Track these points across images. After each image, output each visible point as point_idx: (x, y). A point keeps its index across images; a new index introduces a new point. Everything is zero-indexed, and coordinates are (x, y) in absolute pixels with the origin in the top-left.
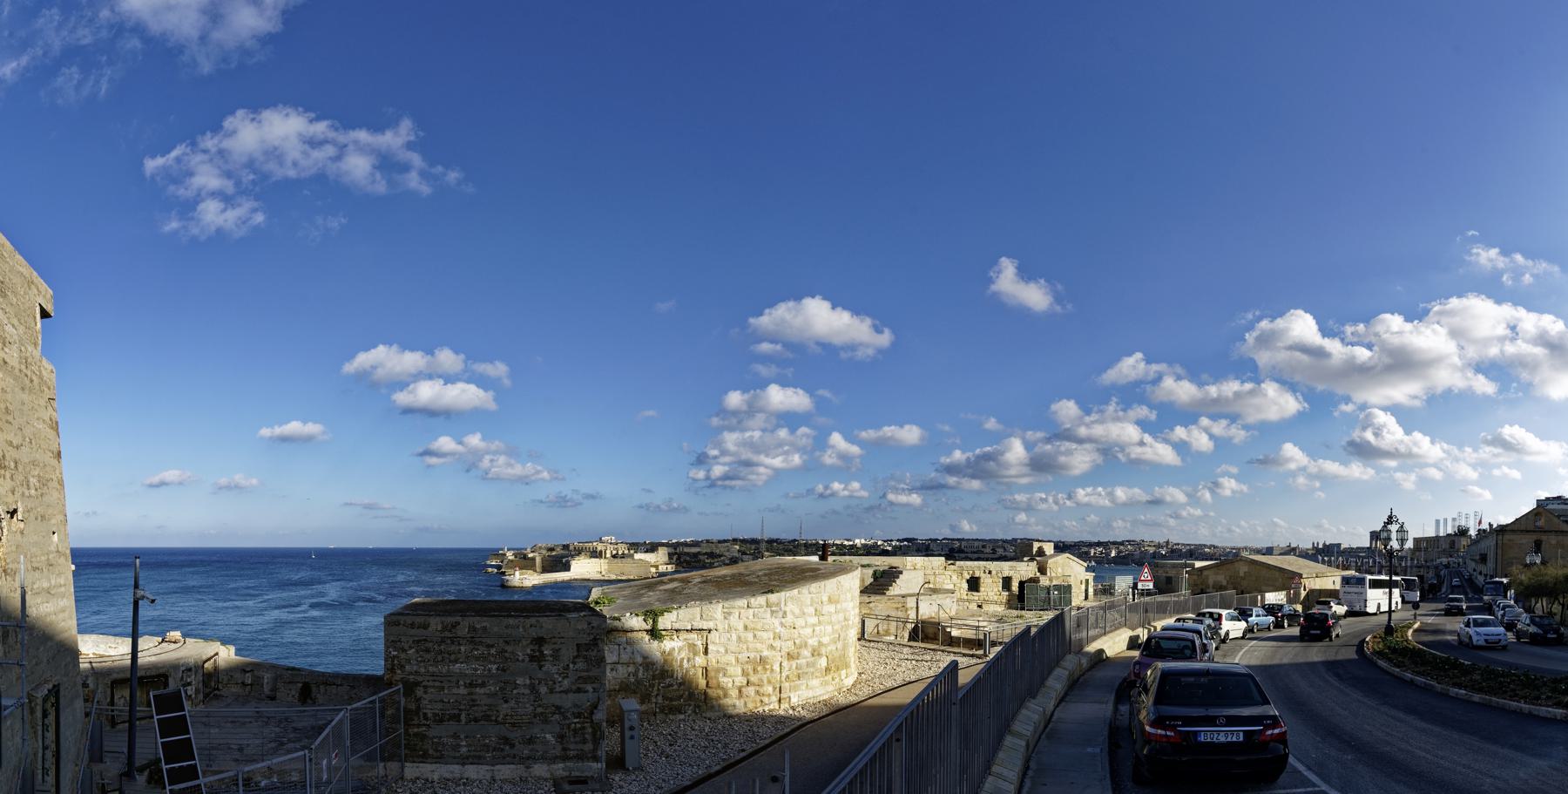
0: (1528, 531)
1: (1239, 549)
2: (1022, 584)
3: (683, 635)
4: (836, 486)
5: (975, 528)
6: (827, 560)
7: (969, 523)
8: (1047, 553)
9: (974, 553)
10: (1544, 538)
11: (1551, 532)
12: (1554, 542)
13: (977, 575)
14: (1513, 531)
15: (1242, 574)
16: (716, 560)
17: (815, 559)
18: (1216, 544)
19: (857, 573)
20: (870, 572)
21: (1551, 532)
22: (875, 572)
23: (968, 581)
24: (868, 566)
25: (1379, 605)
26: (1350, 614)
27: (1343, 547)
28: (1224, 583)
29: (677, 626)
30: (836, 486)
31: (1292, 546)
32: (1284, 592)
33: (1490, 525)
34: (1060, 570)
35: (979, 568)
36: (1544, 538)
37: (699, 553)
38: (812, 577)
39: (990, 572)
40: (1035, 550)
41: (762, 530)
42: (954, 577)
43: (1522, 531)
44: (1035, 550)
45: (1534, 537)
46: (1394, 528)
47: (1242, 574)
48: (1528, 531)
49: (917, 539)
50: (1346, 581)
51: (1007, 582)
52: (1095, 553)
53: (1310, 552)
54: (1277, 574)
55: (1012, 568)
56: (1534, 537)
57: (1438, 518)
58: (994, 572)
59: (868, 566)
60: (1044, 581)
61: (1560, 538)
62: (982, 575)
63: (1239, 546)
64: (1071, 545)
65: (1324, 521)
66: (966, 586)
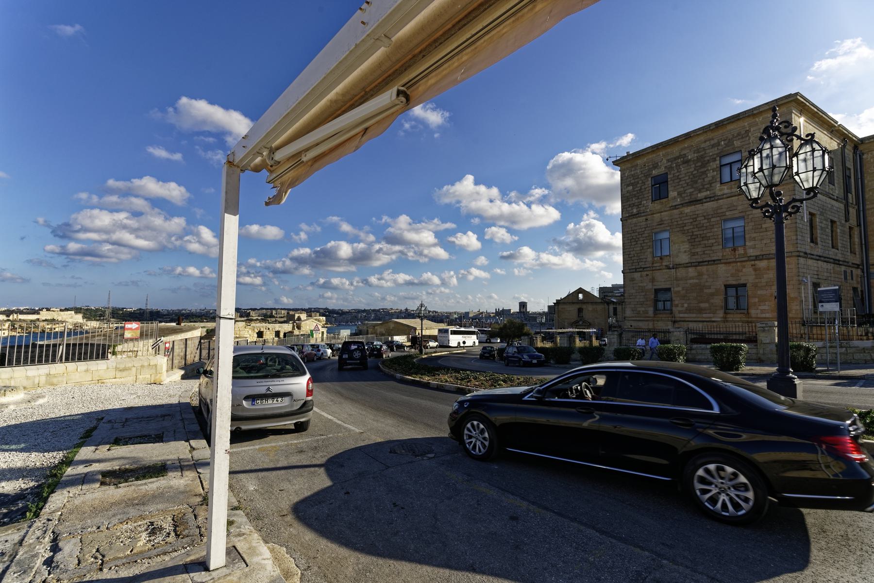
0: (573, 303)
1: (451, 313)
2: (285, 334)
3: (126, 354)
4: (192, 270)
5: (291, 301)
6: (180, 325)
7: (287, 298)
8: (302, 319)
9: (282, 317)
10: (584, 307)
11: (588, 303)
12: (590, 309)
13: (262, 330)
14: (564, 303)
15: (391, 328)
16: (57, 325)
17: (174, 324)
18: (437, 310)
19: (200, 329)
20: (205, 330)
21: (588, 303)
22: (207, 330)
23: (257, 333)
24: (204, 327)
25: (474, 342)
26: (441, 346)
27: (512, 311)
28: (384, 332)
29: (124, 350)
30: (192, 270)
31: (481, 311)
32: (406, 336)
33: (523, 305)
34: (308, 327)
35: (263, 327)
36: (584, 307)
37: (38, 320)
38: (870, 139)
39: (269, 329)
40: (296, 318)
41: (109, 298)
42: (250, 332)
43: (570, 303)
44: (296, 318)
45: (578, 306)
46: (423, 309)
47: (391, 328)
48: (573, 303)
49: (241, 309)
50: (440, 331)
51: (277, 334)
52: (361, 317)
53: (492, 315)
54: (406, 328)
55: (280, 327)
56: (578, 306)
57: (523, 300)
58: (271, 329)
59: (204, 327)
60: (296, 332)
61: (595, 306)
62: (265, 330)
63: (451, 311)
64: (346, 312)
65: (493, 294)
66: (256, 335)
